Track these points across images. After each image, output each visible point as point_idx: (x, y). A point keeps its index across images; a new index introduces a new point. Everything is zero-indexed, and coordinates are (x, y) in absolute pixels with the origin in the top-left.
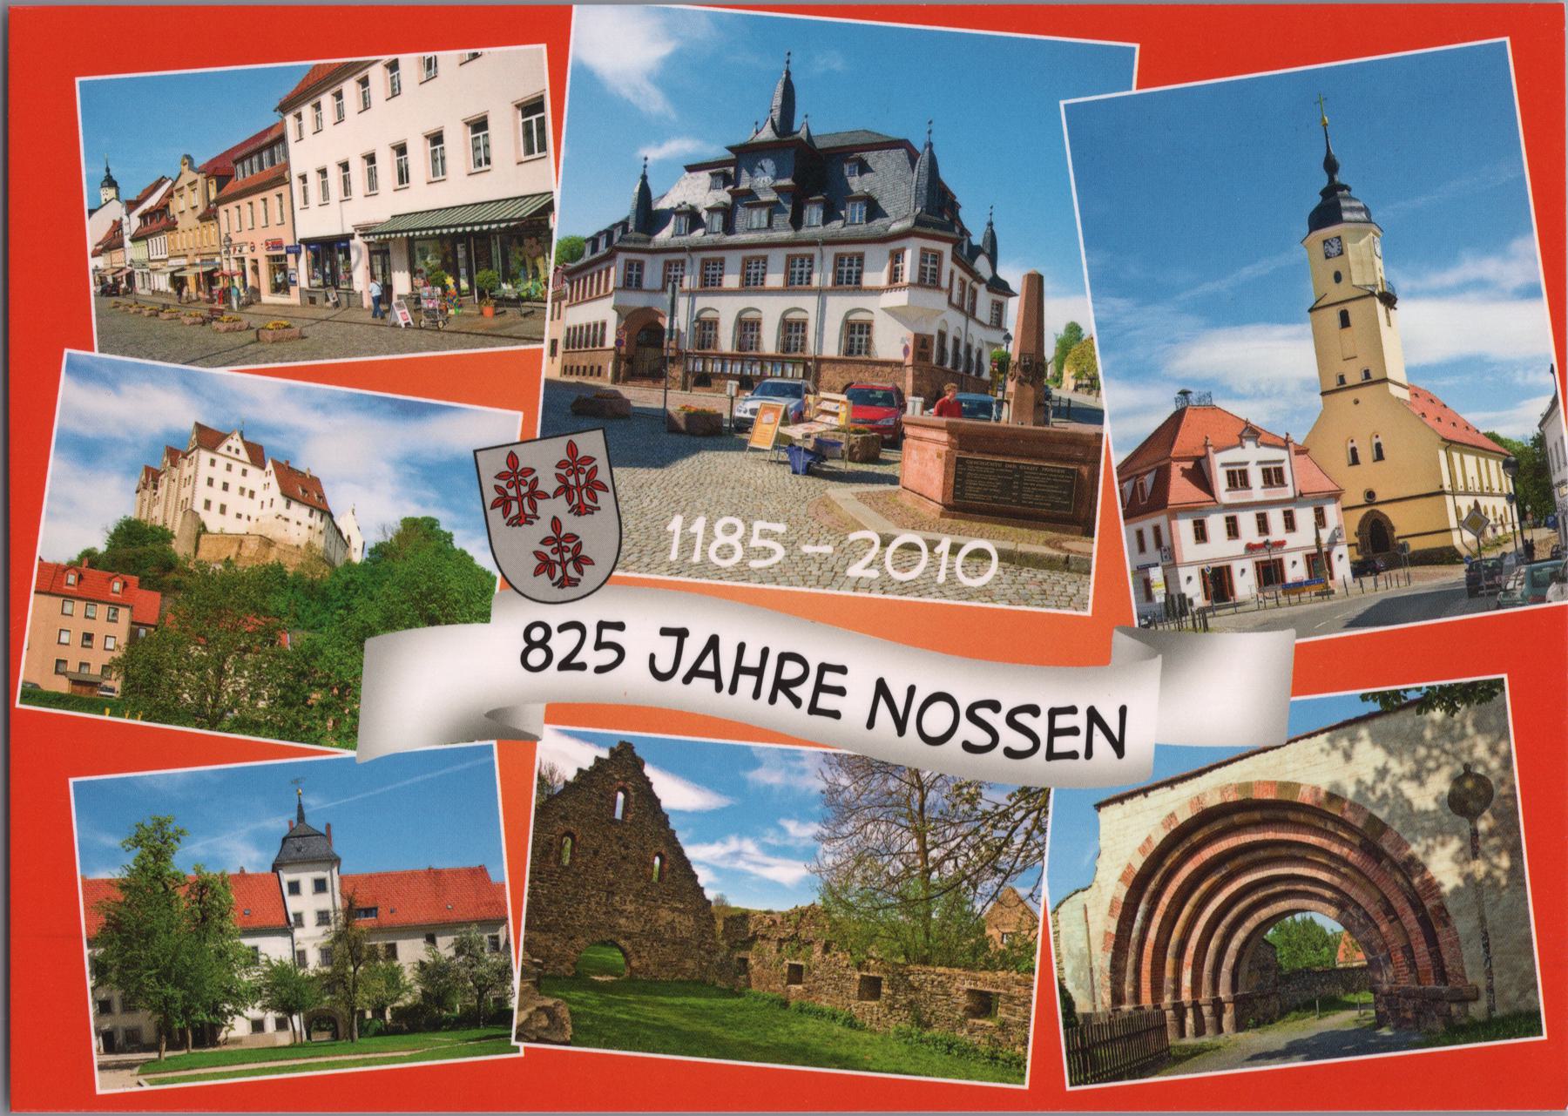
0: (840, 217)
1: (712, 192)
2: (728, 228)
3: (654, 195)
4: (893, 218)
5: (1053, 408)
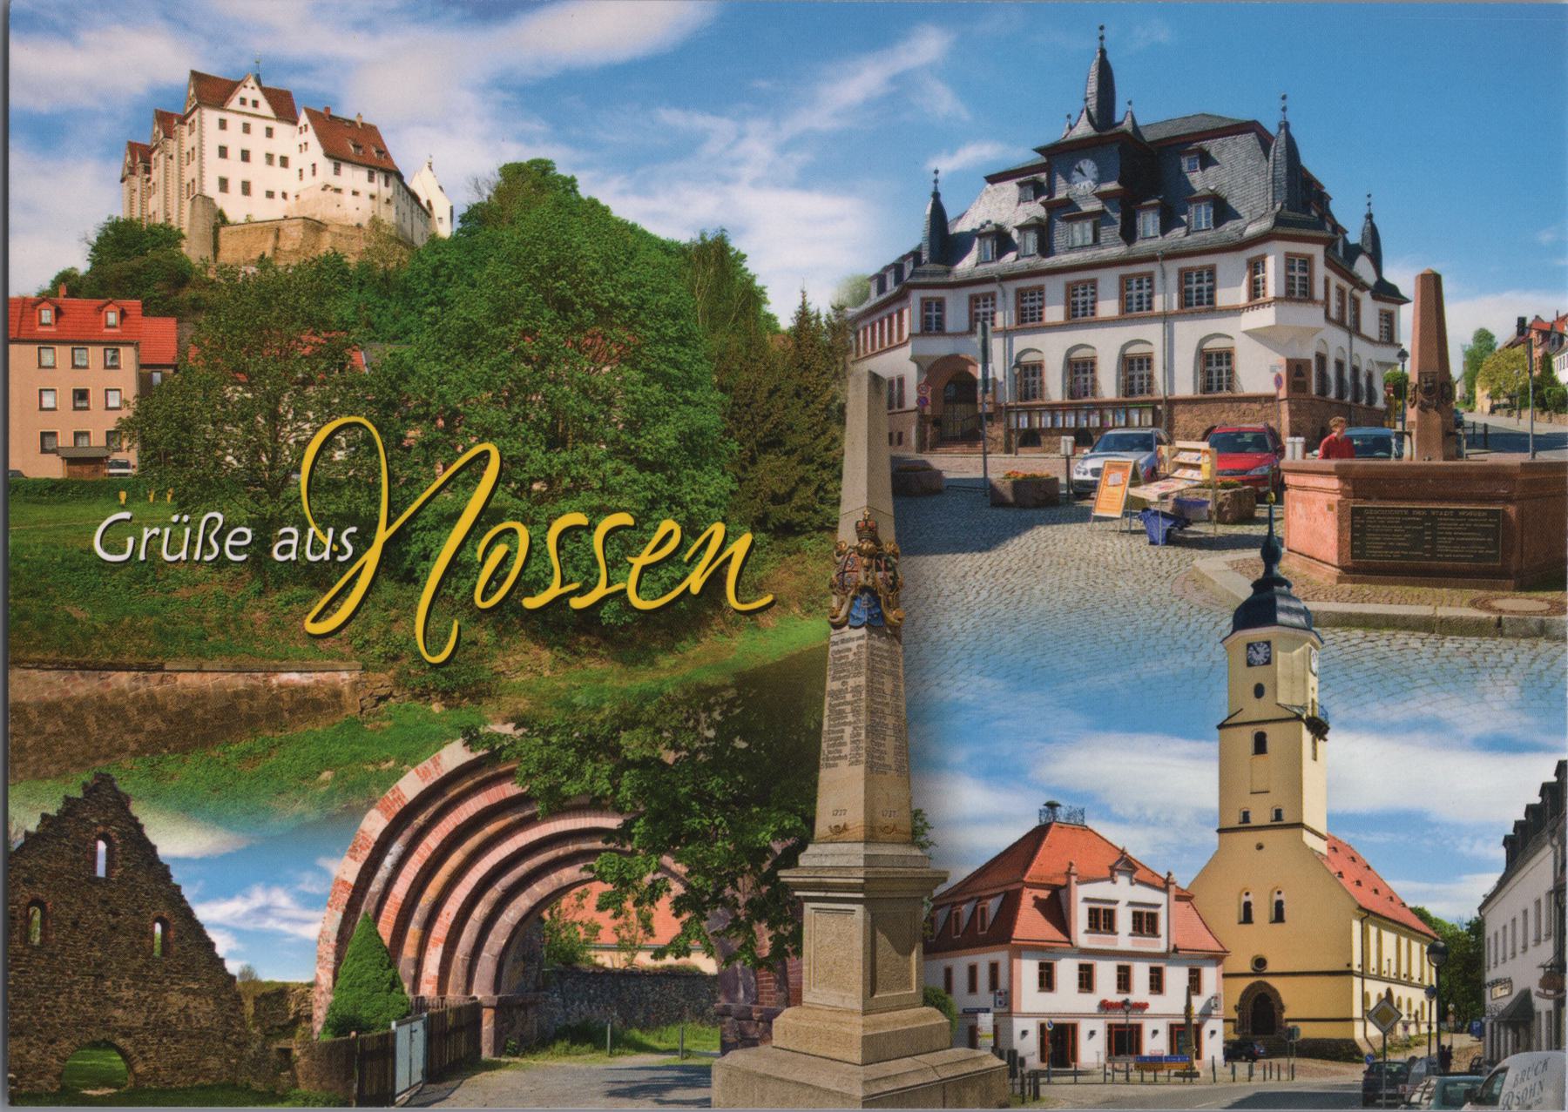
0: (1181, 224)
1: (1022, 206)
2: (1045, 249)
3: (950, 216)
4: (1247, 218)
5: (1467, 436)
